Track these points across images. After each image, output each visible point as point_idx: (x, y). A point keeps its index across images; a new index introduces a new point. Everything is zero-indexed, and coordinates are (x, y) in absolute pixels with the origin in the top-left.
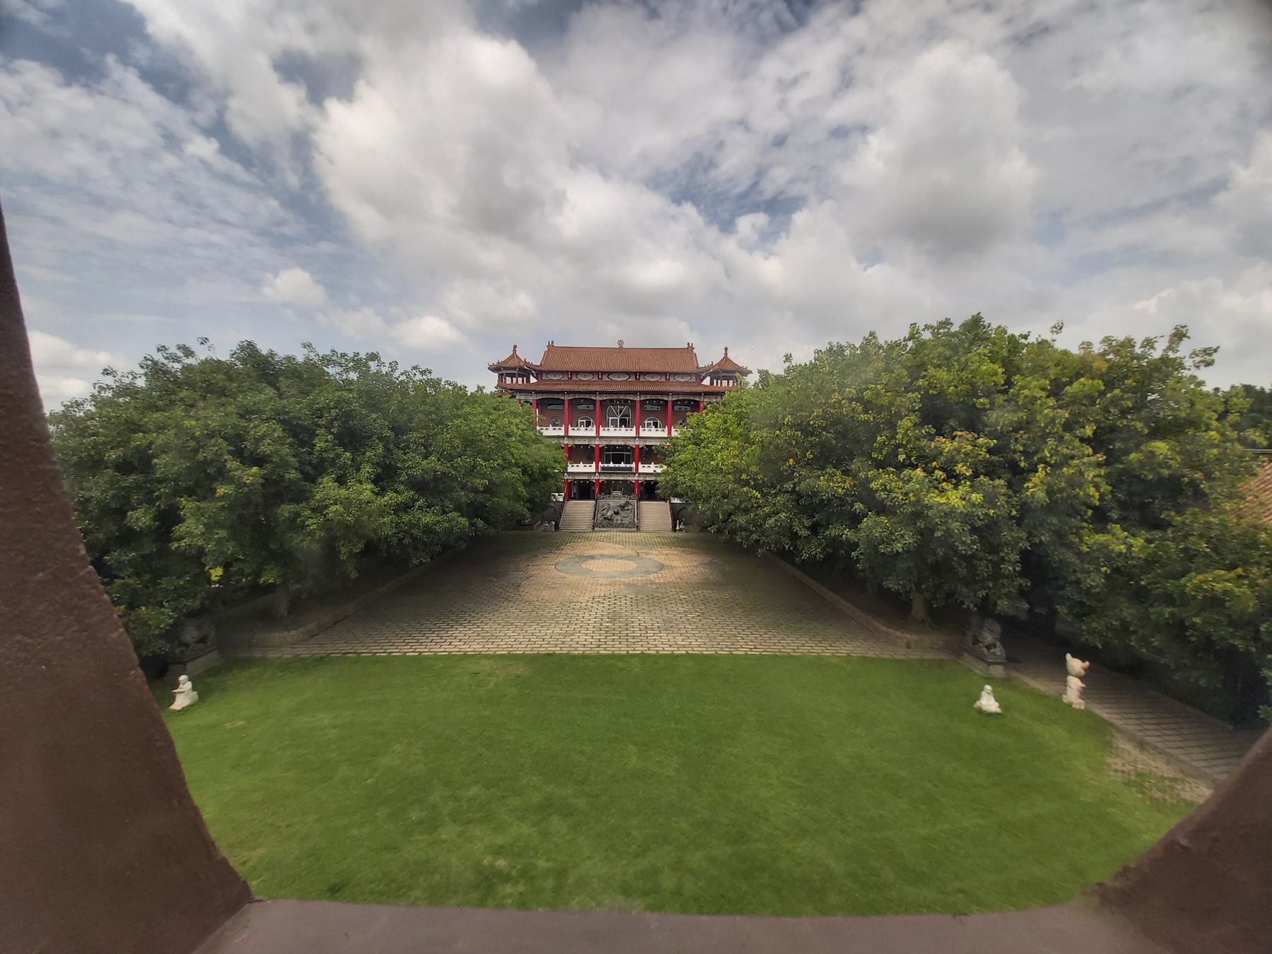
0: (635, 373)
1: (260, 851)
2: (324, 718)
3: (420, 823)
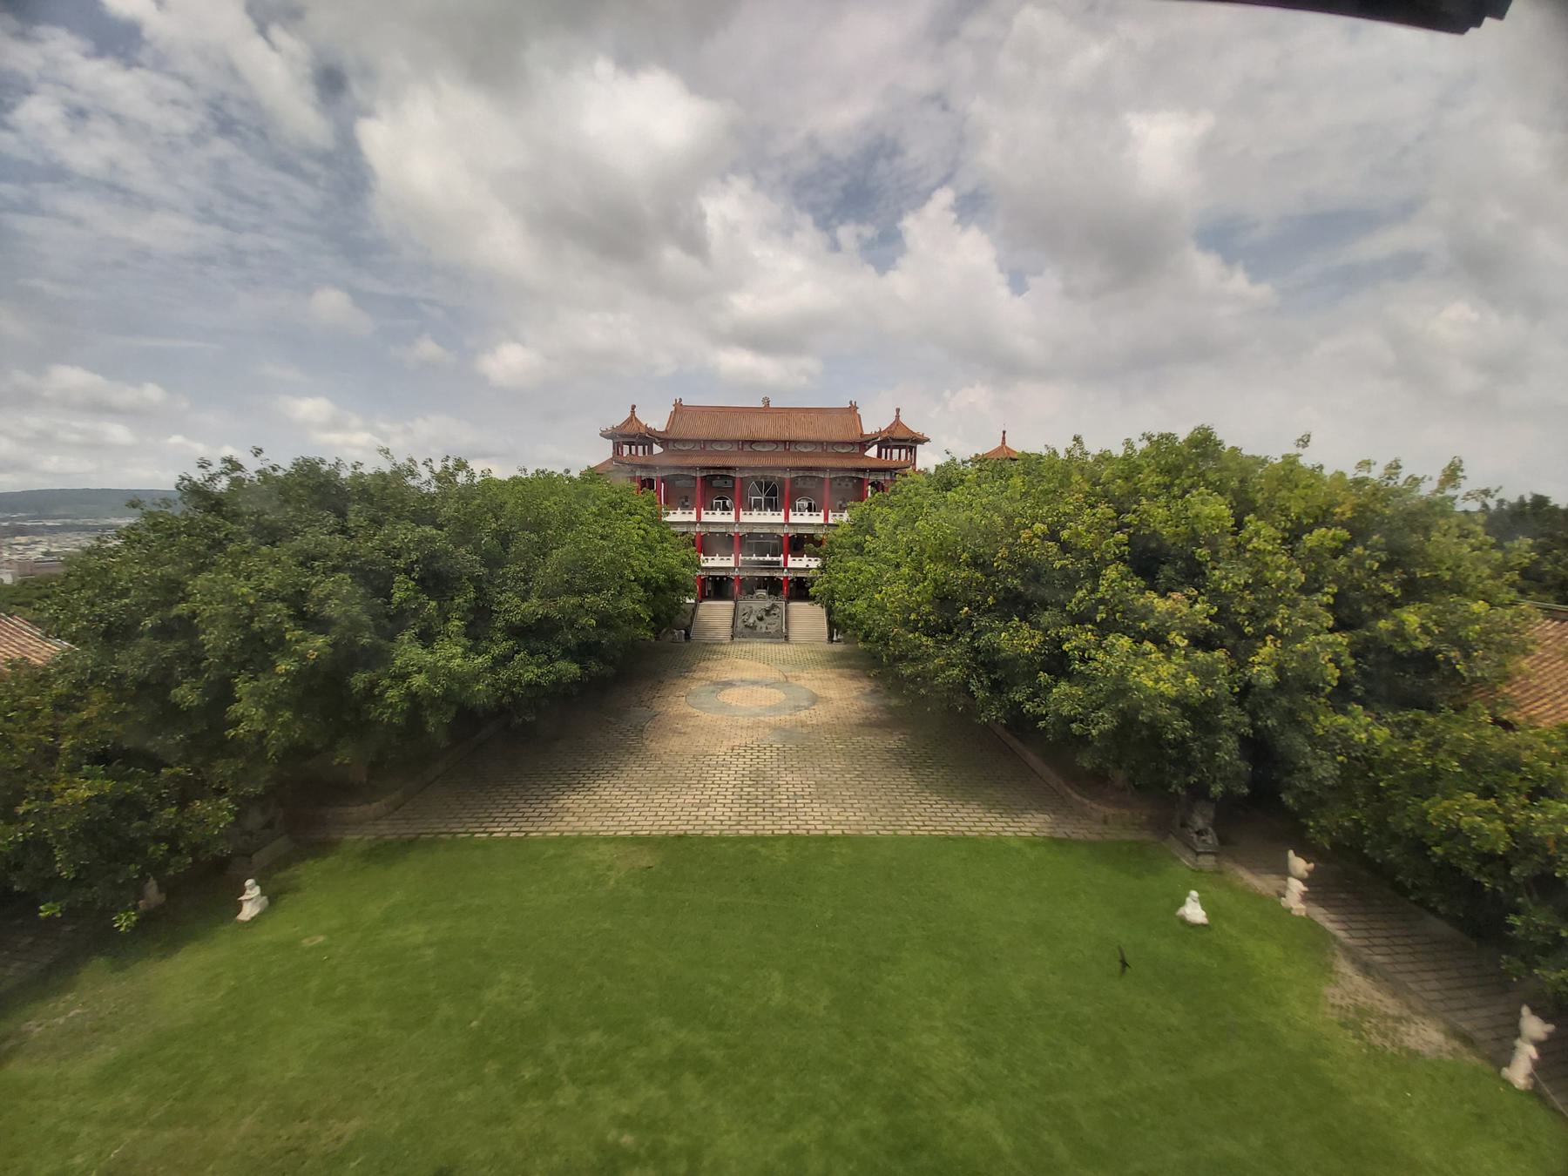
0: (784, 442)
1: (355, 1123)
2: (416, 933)
3: (535, 1084)
